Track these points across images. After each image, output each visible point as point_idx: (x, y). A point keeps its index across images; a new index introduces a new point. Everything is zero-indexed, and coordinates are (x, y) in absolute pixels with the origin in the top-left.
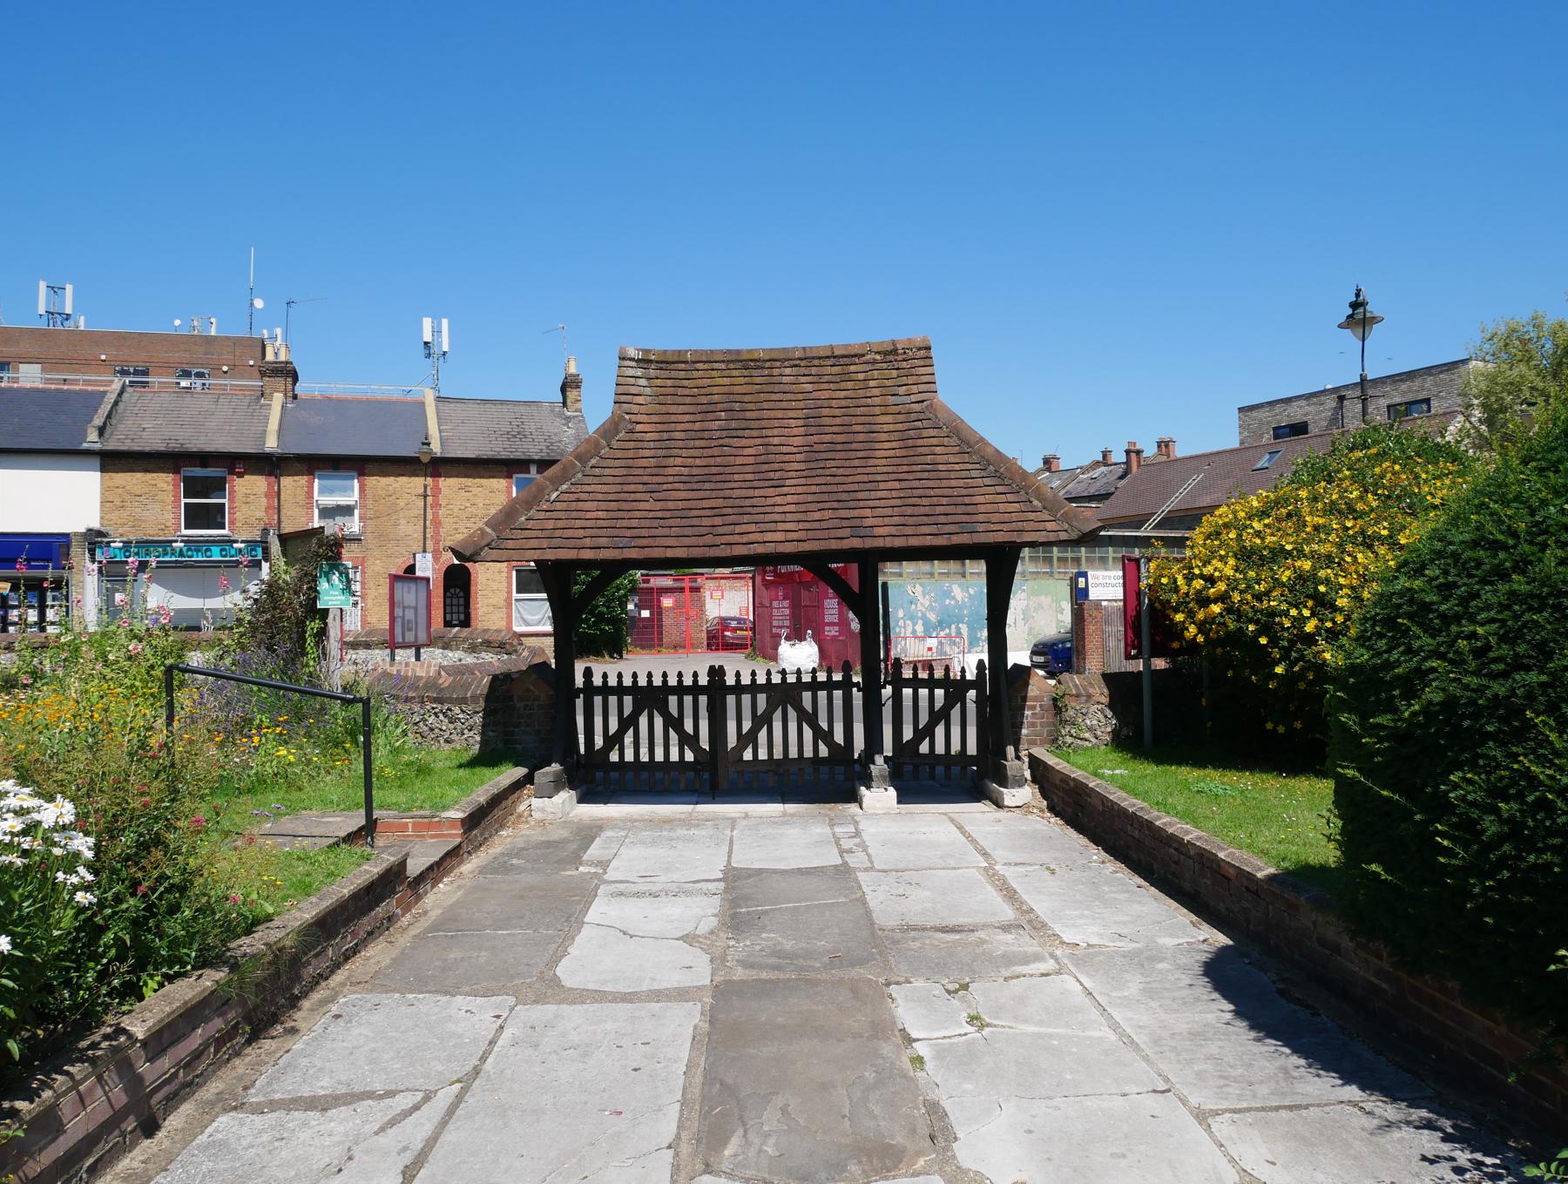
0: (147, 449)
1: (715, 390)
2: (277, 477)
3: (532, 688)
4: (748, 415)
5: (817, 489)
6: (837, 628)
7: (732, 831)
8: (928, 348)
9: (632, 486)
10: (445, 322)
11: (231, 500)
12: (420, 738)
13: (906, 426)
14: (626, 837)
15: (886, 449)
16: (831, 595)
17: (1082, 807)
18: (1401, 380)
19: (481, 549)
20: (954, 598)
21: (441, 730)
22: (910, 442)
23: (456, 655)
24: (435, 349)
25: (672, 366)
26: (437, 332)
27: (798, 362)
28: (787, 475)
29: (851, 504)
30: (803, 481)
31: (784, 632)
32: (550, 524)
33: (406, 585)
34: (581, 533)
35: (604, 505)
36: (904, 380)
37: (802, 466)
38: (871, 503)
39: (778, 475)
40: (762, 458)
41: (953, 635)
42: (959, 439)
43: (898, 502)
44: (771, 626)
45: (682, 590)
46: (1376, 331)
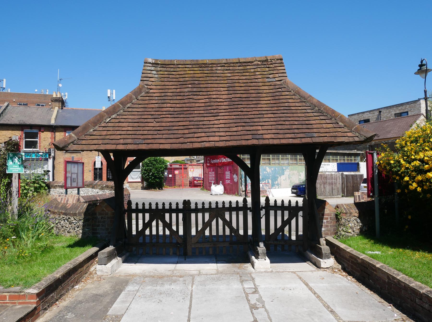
0: (13, 123)
1: (187, 76)
2: (55, 133)
3: (105, 209)
4: (202, 86)
5: (235, 117)
6: (230, 181)
7: (192, 287)
8: (281, 59)
9: (146, 116)
10: (114, 91)
11: (40, 140)
12: (58, 230)
13: (274, 91)
14: (138, 291)
15: (264, 103)
16: (228, 170)
17: (369, 275)
18: (399, 106)
19: (69, 144)
20: (267, 171)
21: (66, 227)
22: (277, 97)
23: (96, 191)
24: (111, 99)
25: (168, 66)
26: (112, 94)
27: (224, 65)
28: (219, 111)
29: (251, 124)
30: (227, 114)
31: (213, 182)
32: (104, 133)
33: (73, 165)
34: (119, 137)
35: (131, 124)
36: (272, 72)
37: (227, 107)
38: (261, 124)
39: (215, 111)
40: (208, 104)
41: (267, 183)
42: (300, 96)
43: (274, 123)
44: (209, 180)
45: (181, 169)
46: (429, 74)
